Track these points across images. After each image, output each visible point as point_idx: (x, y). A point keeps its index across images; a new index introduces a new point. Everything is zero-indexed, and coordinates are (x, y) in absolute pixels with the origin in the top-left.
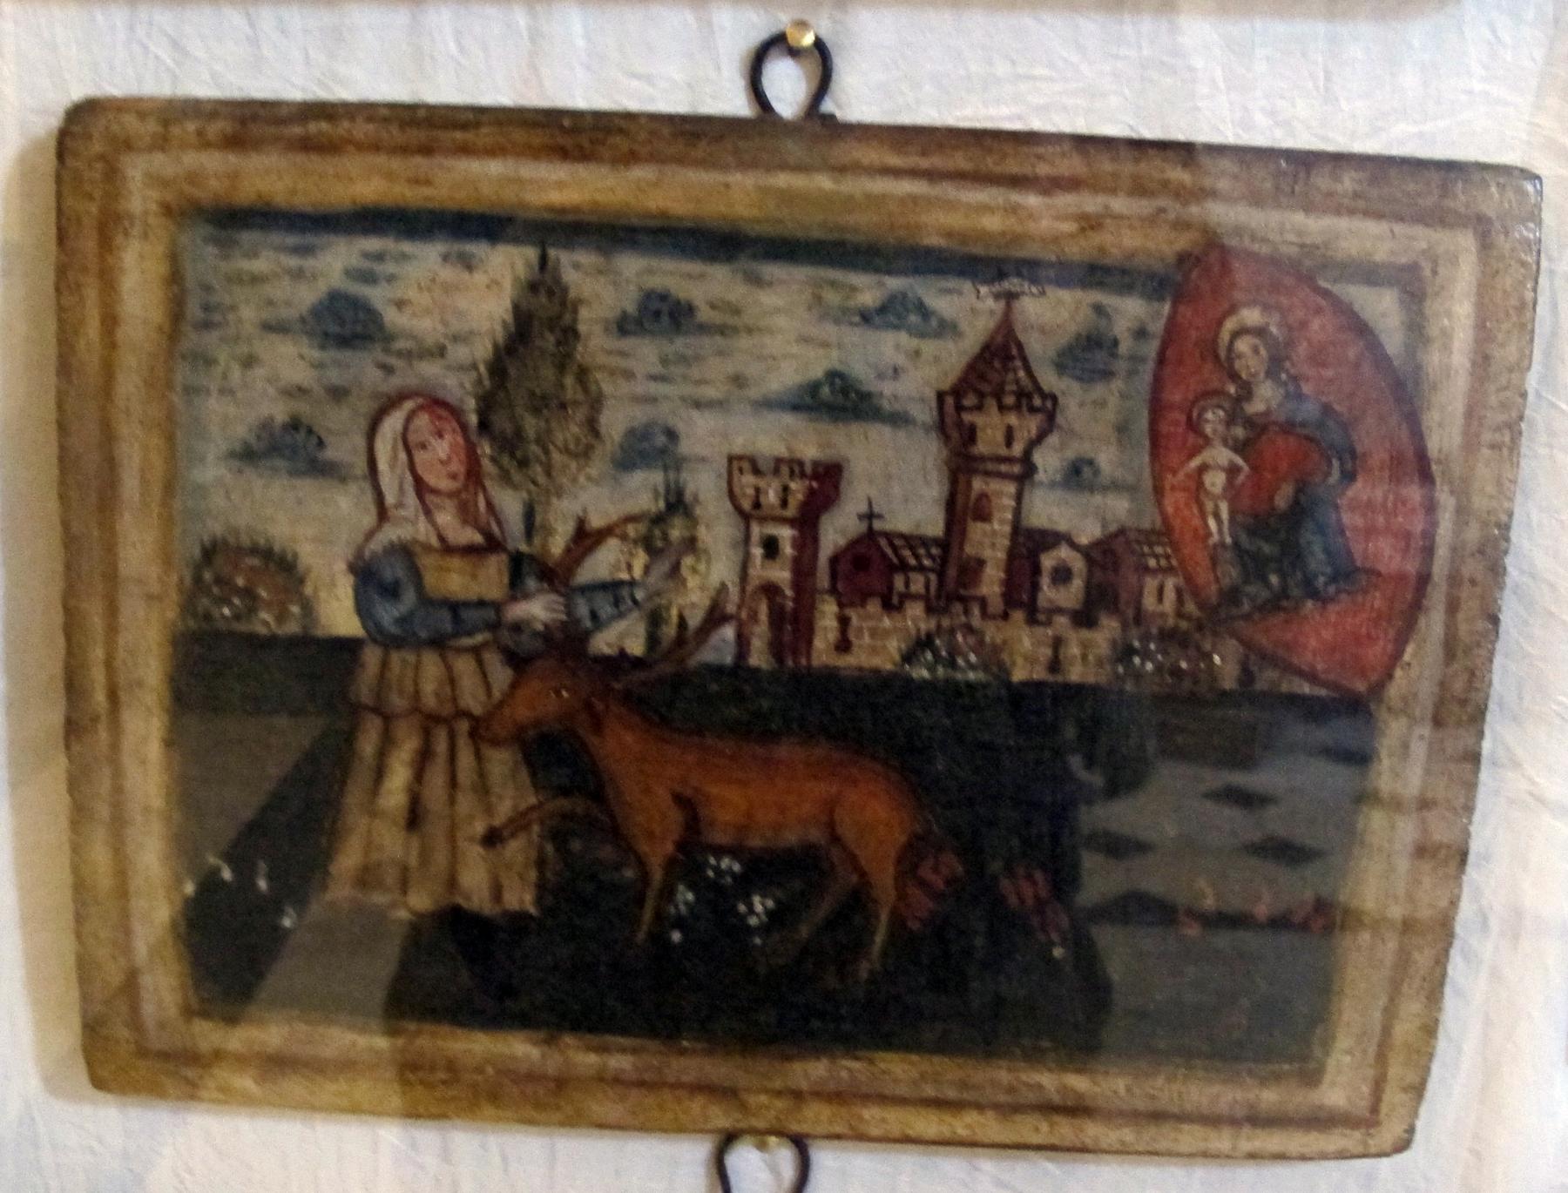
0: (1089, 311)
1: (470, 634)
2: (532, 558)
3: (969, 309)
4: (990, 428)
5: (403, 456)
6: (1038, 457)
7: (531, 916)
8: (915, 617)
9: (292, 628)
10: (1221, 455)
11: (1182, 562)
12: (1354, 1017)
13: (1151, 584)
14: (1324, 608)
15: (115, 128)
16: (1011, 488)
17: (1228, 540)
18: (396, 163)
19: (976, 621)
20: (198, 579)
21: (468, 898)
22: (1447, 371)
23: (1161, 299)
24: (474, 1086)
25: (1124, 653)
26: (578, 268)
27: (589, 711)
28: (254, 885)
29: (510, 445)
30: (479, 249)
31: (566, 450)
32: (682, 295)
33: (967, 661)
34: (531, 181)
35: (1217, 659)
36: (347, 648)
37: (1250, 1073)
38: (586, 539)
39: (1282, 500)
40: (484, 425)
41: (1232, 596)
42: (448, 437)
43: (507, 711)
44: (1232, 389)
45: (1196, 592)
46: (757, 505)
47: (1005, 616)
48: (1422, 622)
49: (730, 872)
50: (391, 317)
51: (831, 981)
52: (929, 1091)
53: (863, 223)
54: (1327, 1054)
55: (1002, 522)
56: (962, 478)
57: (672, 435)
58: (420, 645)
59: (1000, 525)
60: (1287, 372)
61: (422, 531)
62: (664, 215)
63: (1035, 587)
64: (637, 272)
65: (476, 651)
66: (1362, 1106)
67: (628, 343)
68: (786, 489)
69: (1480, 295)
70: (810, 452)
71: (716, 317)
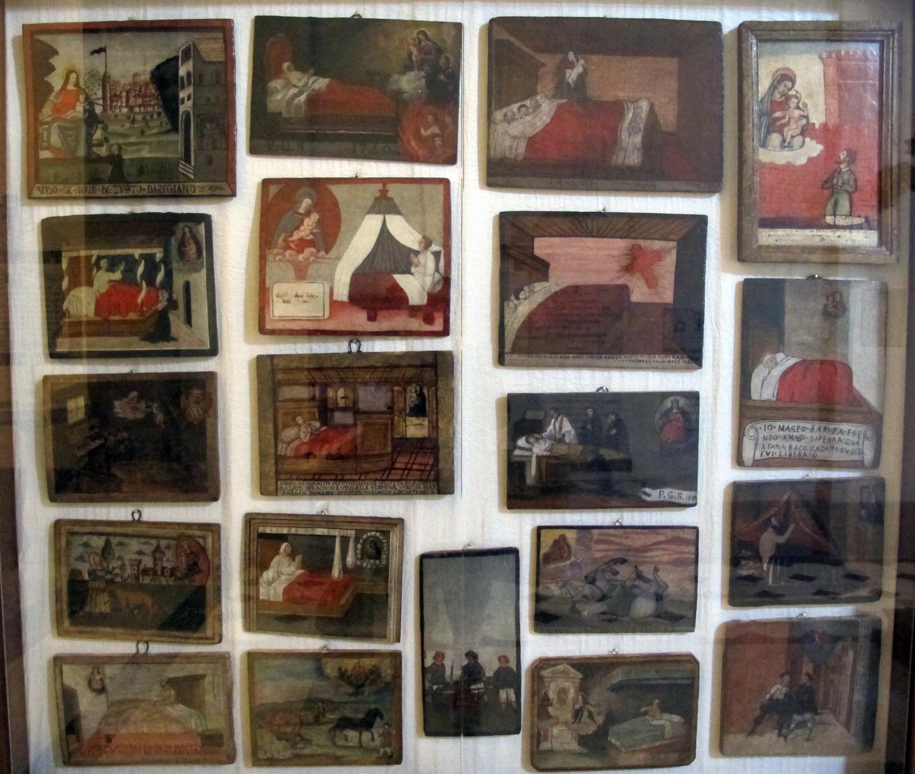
3: (154, 542)
4: (158, 555)
8: (151, 577)
38: (114, 568)
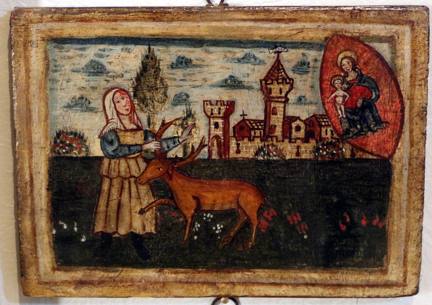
0: (301, 55)
1: (134, 154)
2: (150, 131)
3: (267, 56)
4: (275, 89)
5: (113, 105)
6: (289, 96)
7: (154, 234)
8: (258, 143)
9: (83, 154)
10: (340, 93)
11: (332, 124)
12: (395, 251)
13: (324, 130)
14: (373, 134)
15: (27, 17)
16: (282, 105)
17: (345, 116)
18: (107, 24)
19: (275, 143)
20: (55, 142)
21: (136, 230)
22: (404, 65)
23: (321, 50)
24: (139, 286)
25: (317, 149)
26: (159, 51)
27: (169, 172)
28: (74, 230)
29: (143, 100)
30: (131, 47)
31: (158, 101)
32: (188, 57)
33: (273, 154)
34: (145, 28)
35: (344, 150)
36: (100, 159)
37: (366, 271)
39: (359, 103)
40: (135, 95)
41: (347, 132)
42: (125, 99)
43: (145, 175)
44: (342, 74)
45: (336, 131)
46: (212, 114)
47: (283, 141)
48: (403, 136)
49: (210, 218)
50: (109, 67)
51: (240, 249)
52: (272, 281)
53: (237, 35)
54: (388, 264)
55: (280, 115)
56: (268, 103)
57: (188, 96)
58: (119, 158)
59: (280, 115)
60: (358, 68)
61: (119, 126)
62: (182, 35)
63: (291, 133)
64: (174, 52)
65: (135, 158)
66: (401, 280)
67: (174, 71)
68: (220, 109)
69: (412, 43)
70: (226, 98)
71: (198, 63)
